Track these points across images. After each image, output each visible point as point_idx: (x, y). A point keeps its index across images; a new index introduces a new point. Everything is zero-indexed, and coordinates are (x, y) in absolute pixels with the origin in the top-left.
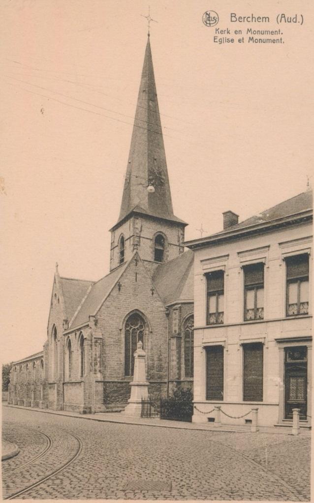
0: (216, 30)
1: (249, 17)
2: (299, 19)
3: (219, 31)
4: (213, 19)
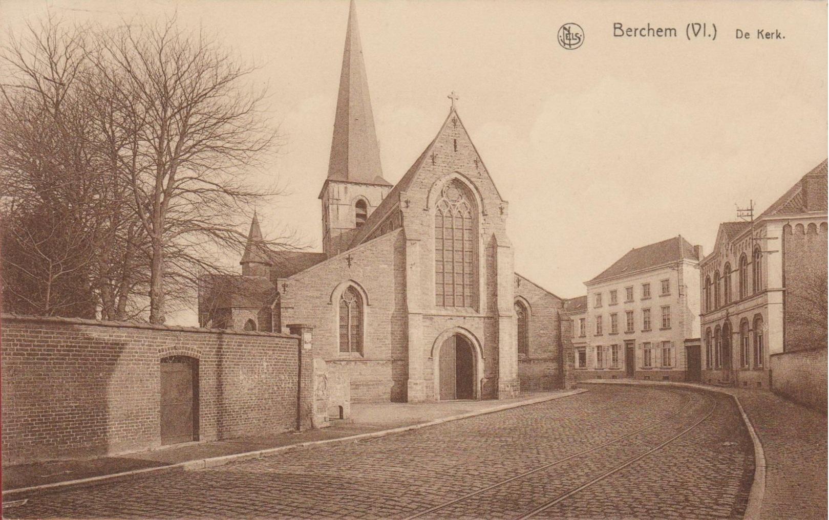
0: (759, 33)
1: (644, 29)
2: (710, 30)
3: (764, 33)
4: (575, 37)
